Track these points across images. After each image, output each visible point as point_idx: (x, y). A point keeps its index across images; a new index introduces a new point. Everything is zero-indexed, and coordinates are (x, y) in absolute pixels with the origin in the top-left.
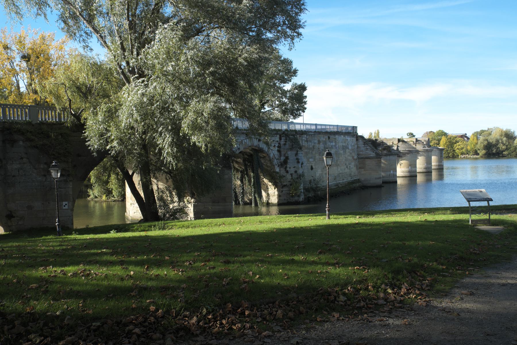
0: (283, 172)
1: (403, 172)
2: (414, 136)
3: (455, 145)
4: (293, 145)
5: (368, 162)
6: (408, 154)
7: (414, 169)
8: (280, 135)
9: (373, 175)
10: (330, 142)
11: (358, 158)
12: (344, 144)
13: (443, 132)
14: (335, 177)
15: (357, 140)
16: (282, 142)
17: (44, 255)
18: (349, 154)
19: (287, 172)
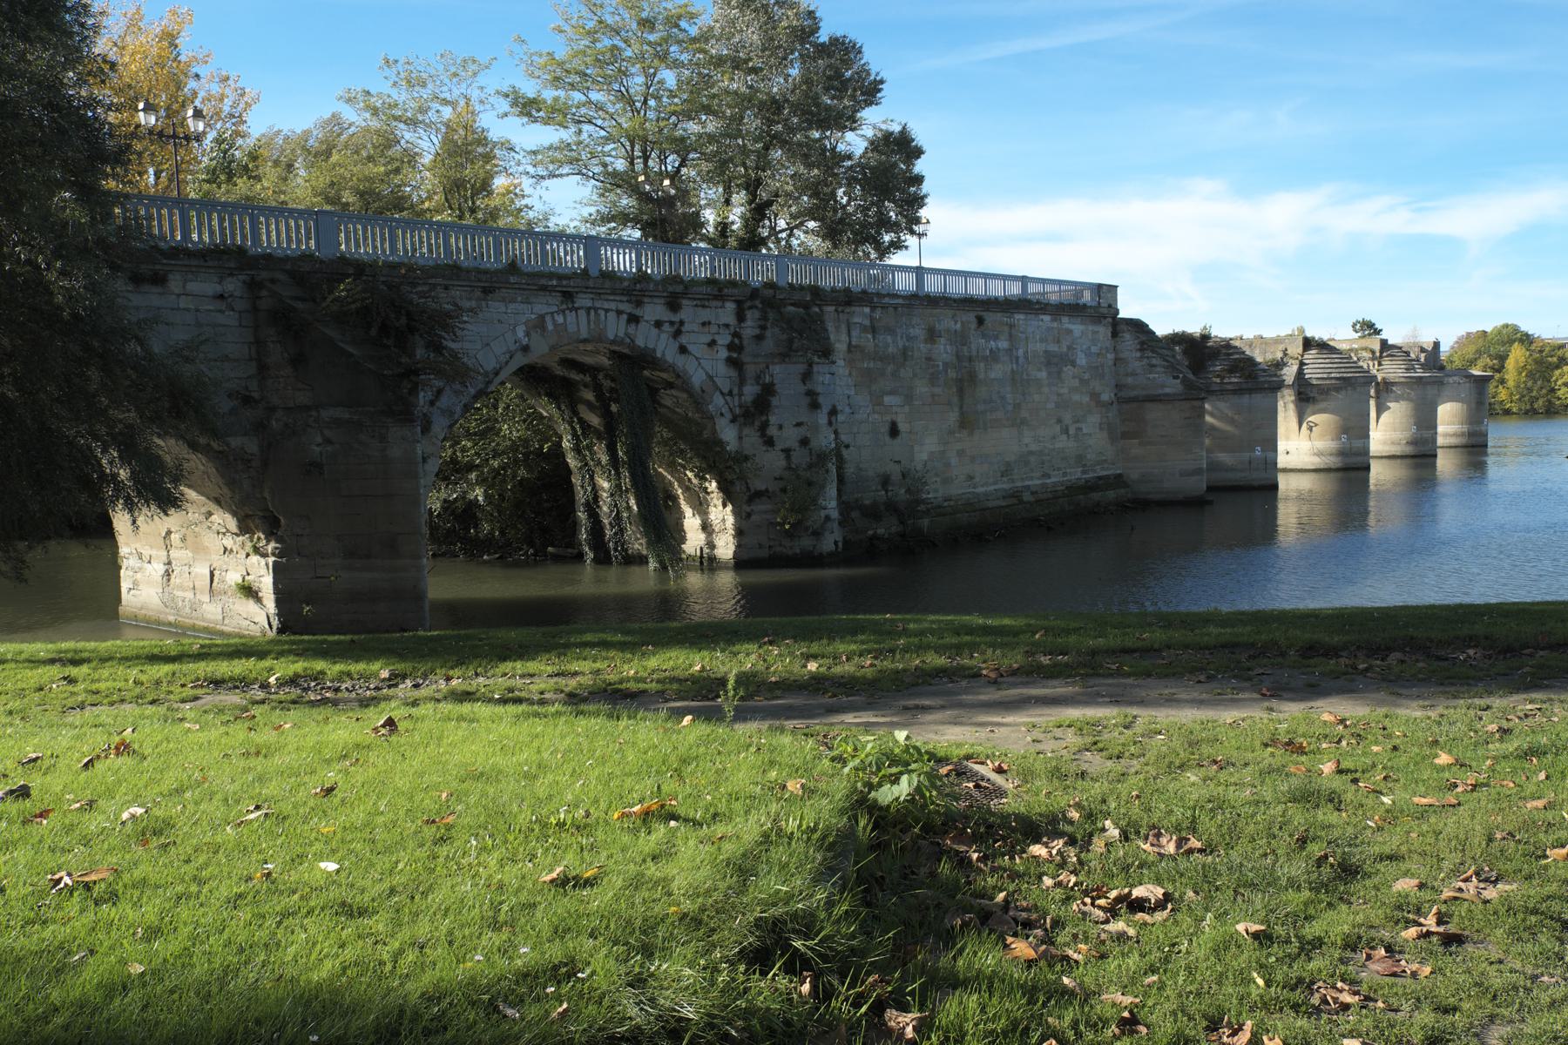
0: (752, 438)
1: (1319, 454)
2: (1378, 332)
3: (1557, 372)
4: (791, 341)
5: (1154, 413)
6: (1338, 389)
7: (1357, 444)
8: (739, 303)
9: (1170, 463)
10: (984, 336)
11: (1121, 401)
12: (1053, 348)
13: (1516, 329)
14: (1008, 464)
15: (1115, 334)
16: (749, 329)
17: (1006, 639)
18: (1076, 383)
19: (770, 442)
